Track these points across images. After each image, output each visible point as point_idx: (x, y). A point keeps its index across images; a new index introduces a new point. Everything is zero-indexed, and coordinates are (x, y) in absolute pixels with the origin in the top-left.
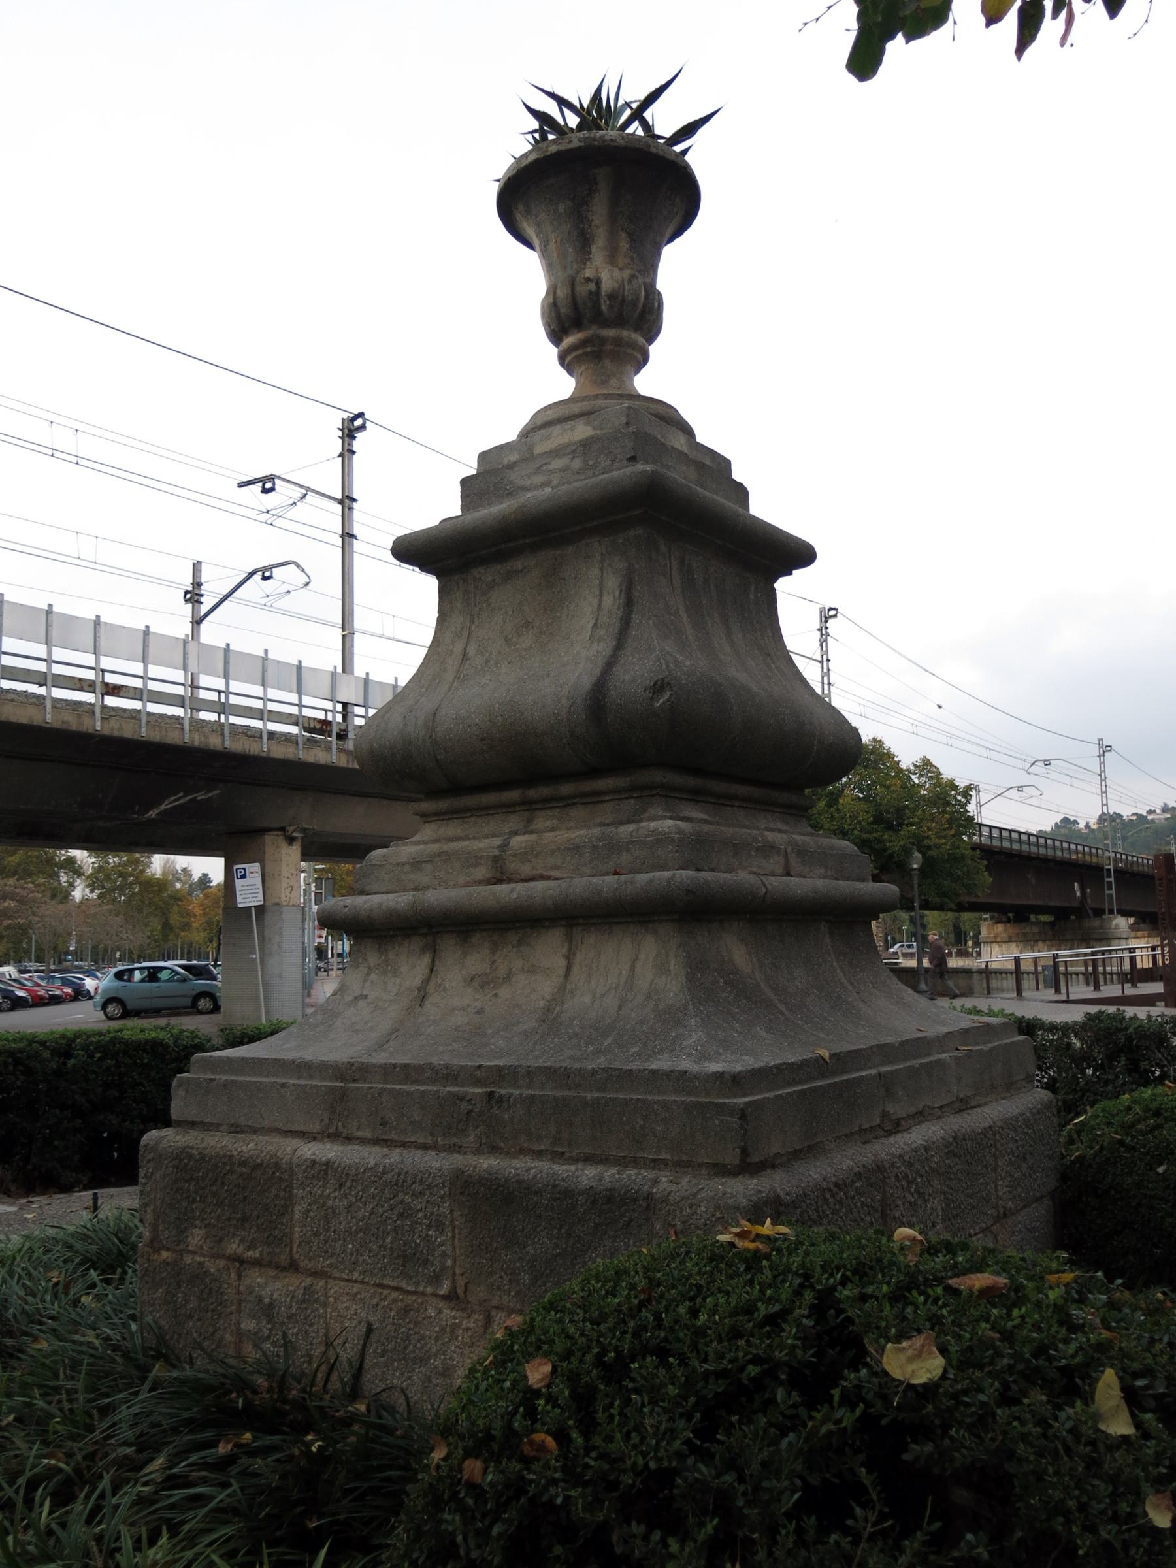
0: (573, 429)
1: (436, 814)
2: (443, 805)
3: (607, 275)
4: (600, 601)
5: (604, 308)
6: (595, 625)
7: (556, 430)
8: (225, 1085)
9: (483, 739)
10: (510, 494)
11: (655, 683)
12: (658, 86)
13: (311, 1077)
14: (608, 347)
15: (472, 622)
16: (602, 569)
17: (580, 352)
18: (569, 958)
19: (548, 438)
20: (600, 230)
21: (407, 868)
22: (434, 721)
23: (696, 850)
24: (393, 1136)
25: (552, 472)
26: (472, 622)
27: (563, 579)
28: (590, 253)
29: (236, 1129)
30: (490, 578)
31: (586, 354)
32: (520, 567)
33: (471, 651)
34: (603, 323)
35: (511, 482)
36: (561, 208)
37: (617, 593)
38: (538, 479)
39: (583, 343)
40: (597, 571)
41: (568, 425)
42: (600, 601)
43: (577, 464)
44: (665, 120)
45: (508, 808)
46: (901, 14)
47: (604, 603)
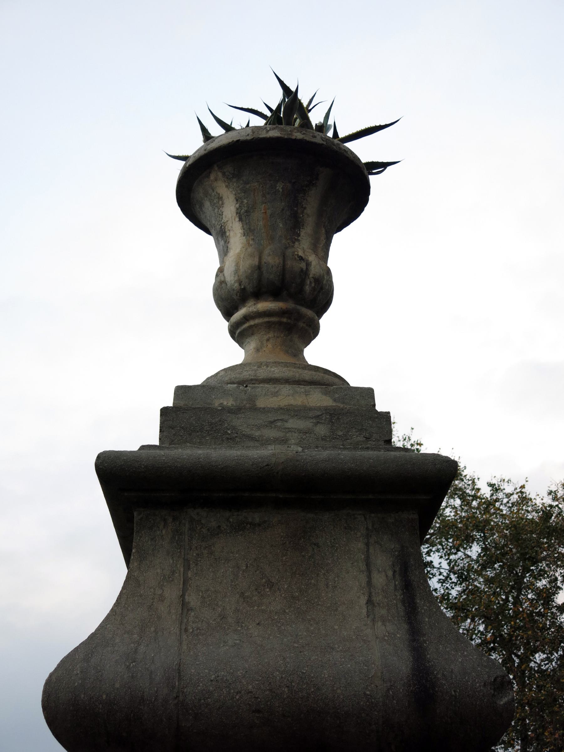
0: (307, 394)
4: (369, 577)
5: (307, 288)
6: (370, 602)
7: (286, 389)
9: (258, 711)
10: (233, 439)
11: (495, 680)
12: (378, 125)
14: (301, 324)
15: (187, 567)
16: (367, 545)
19: (276, 394)
20: (310, 219)
22: (180, 679)
25: (290, 430)
26: (187, 567)
27: (317, 545)
28: (299, 235)
30: (214, 524)
31: (280, 323)
32: (257, 520)
33: (193, 599)
34: (279, 298)
35: (234, 428)
36: (280, 187)
37: (390, 573)
38: (271, 433)
39: (282, 313)
40: (361, 545)
41: (301, 389)
42: (369, 577)
43: (322, 430)
44: (364, 151)
47: (374, 581)
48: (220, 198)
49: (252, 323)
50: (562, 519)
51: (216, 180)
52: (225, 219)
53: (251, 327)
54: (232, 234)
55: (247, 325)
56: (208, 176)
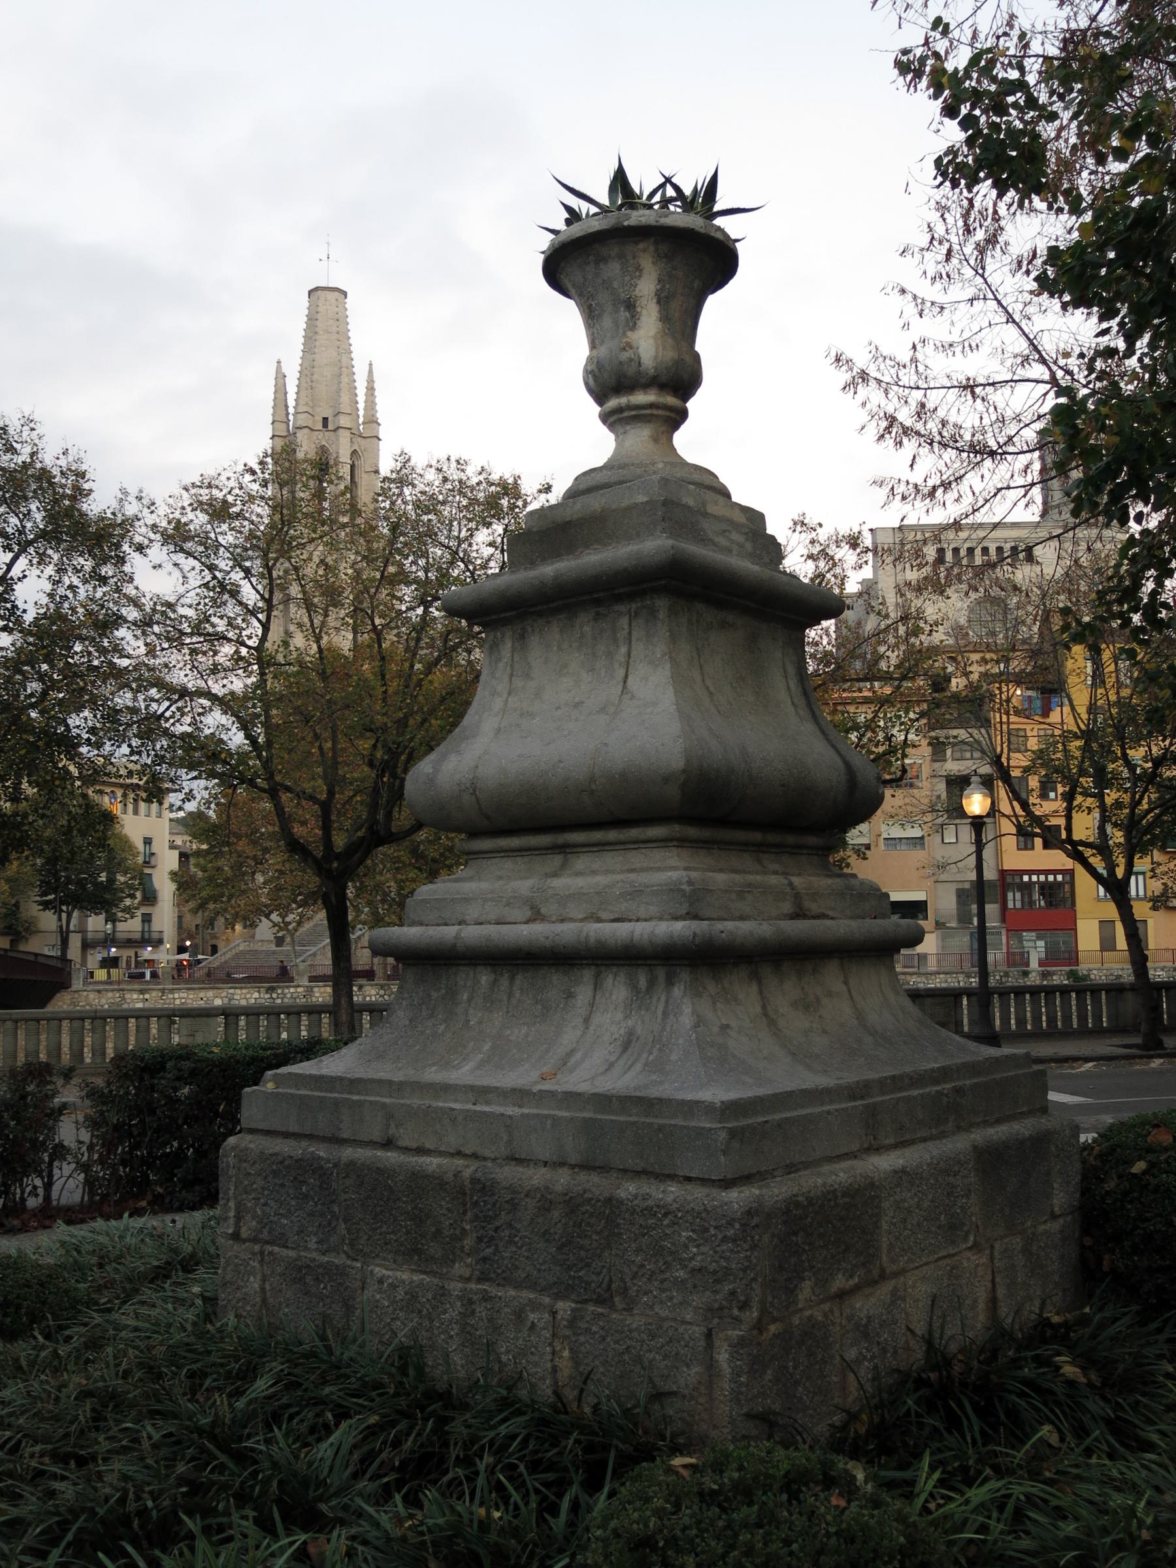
1: (691, 841)
2: (692, 832)
3: (647, 342)
8: (779, 1125)
13: (831, 1102)
17: (673, 415)
18: (846, 983)
21: (734, 896)
23: (693, 903)
24: (908, 1137)
29: (791, 1168)
34: (647, 388)
45: (744, 847)
46: (1117, 439)
48: (639, 269)
49: (655, 412)
50: (1171, 667)
51: (644, 250)
52: (637, 292)
53: (652, 415)
54: (644, 312)
55: (648, 412)
56: (637, 243)
